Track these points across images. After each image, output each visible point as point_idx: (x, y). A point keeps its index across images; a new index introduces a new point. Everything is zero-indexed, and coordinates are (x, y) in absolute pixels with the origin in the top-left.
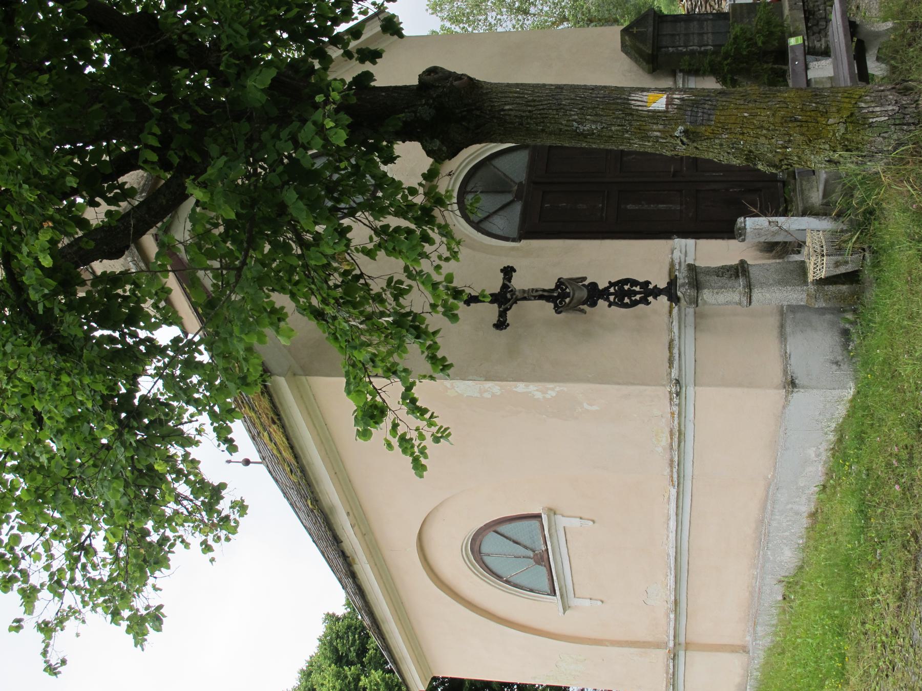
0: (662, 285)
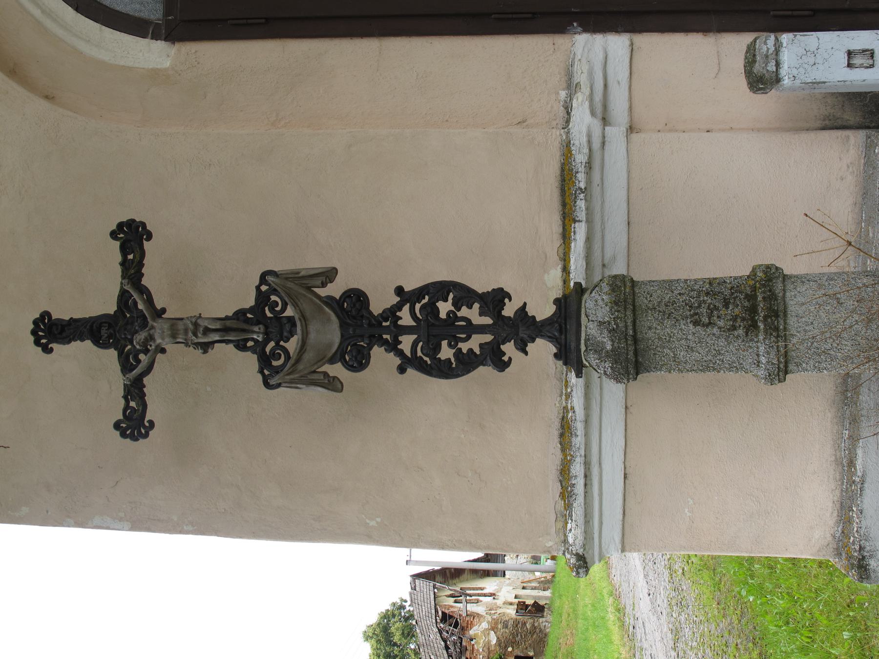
0: (542, 309)
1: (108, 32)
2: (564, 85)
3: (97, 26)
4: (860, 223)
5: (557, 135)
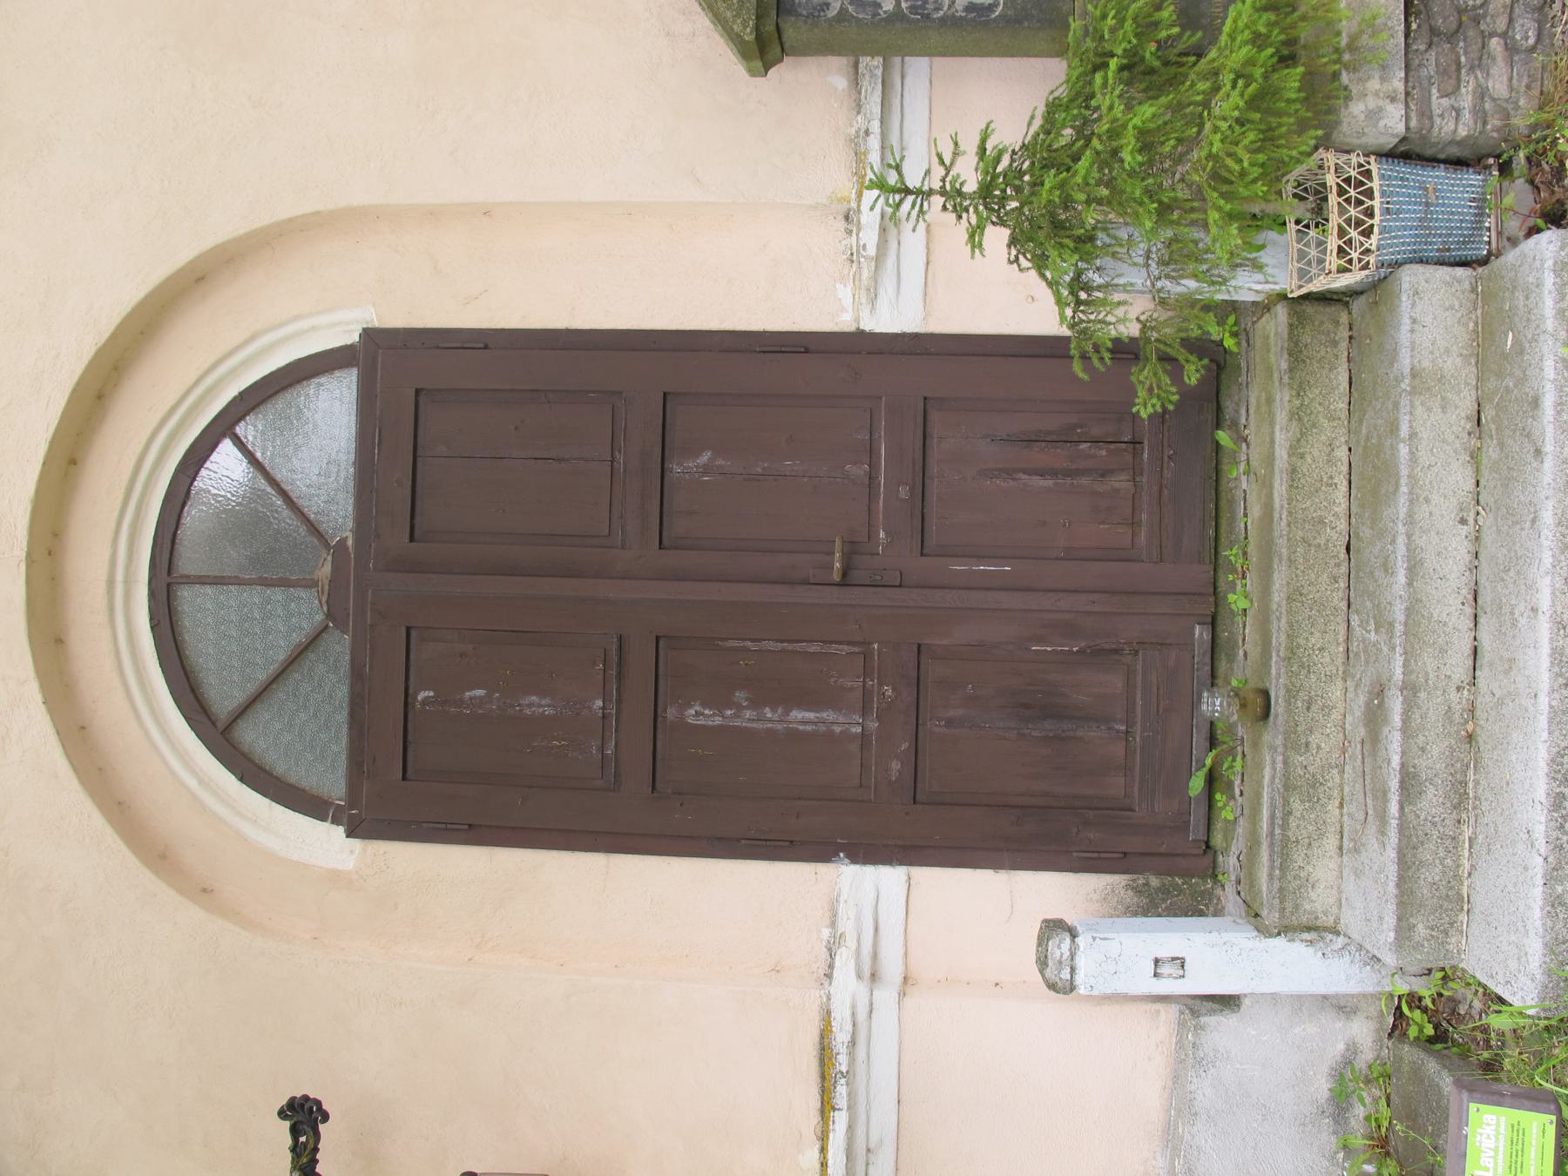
1: (279, 811)
2: (828, 922)
3: (266, 801)
4: (1168, 1111)
5: (814, 998)
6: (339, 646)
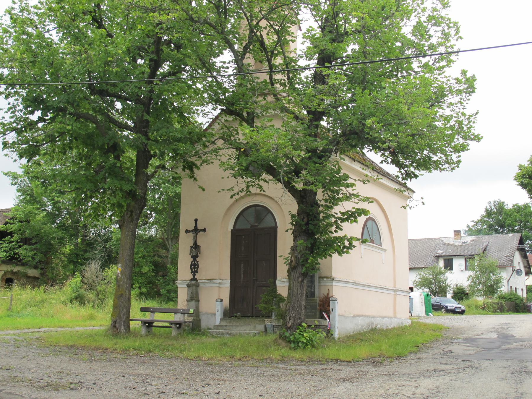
6: (249, 227)
